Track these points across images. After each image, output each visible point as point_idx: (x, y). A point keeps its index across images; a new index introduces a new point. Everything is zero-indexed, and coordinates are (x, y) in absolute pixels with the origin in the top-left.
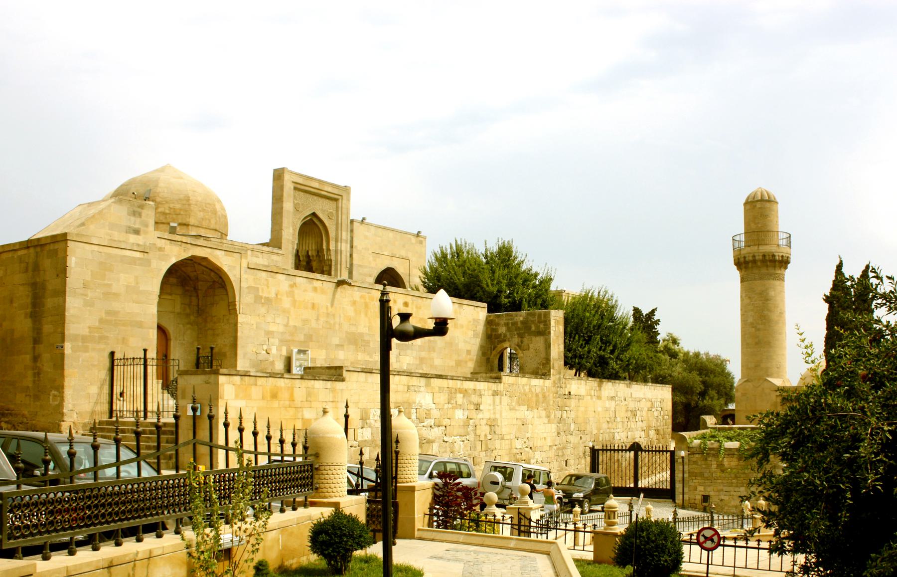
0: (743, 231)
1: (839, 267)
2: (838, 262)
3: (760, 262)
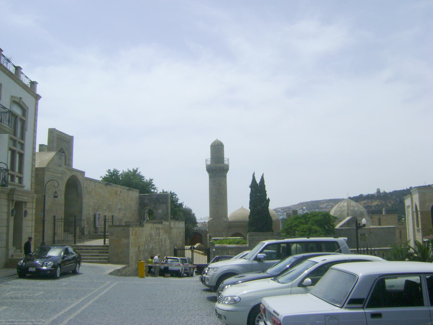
0: (210, 158)
1: (254, 174)
2: (253, 173)
3: (218, 170)
